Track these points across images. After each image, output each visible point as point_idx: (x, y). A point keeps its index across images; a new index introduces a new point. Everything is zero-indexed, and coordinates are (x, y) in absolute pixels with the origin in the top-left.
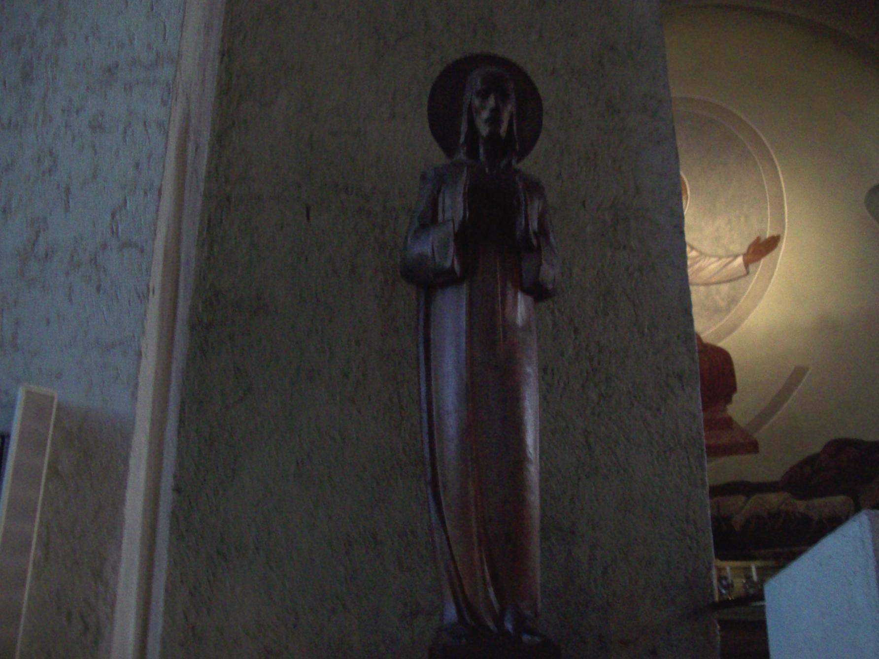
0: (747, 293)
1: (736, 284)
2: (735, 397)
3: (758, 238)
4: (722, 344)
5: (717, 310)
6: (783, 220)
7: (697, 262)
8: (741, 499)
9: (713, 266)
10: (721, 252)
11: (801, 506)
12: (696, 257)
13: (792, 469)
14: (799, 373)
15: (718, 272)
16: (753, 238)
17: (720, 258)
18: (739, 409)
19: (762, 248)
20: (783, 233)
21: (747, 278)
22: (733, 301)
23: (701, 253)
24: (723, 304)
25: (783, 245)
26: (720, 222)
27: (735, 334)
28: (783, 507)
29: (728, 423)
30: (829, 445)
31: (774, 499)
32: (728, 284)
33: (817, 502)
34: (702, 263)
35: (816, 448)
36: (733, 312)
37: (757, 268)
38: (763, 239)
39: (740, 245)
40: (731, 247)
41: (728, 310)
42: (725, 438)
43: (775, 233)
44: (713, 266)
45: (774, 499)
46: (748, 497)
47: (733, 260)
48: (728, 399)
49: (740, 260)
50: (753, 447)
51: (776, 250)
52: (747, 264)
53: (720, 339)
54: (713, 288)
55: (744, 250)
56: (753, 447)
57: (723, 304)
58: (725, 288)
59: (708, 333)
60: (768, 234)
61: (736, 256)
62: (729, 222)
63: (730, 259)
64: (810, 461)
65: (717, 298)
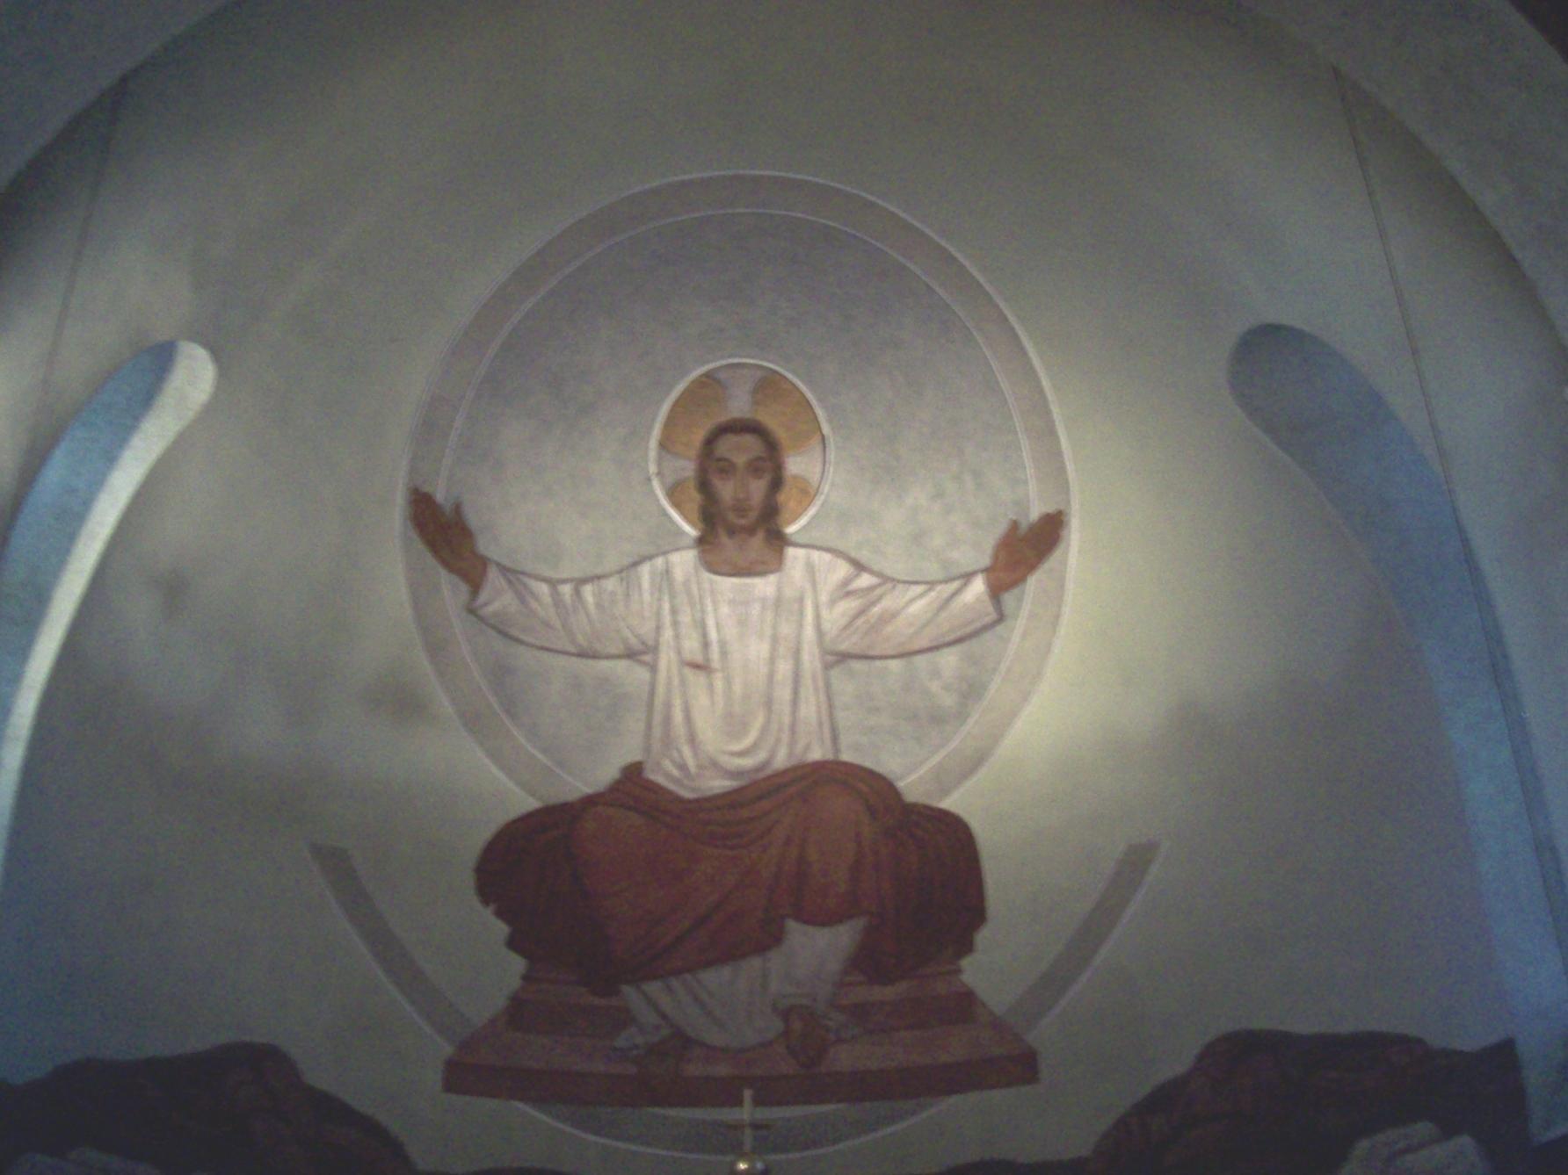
0: (1003, 668)
1: (974, 645)
2: (983, 937)
3: (1015, 525)
4: (947, 804)
5: (937, 718)
6: (1062, 469)
7: (873, 603)
9: (915, 608)
10: (933, 570)
12: (871, 589)
13: (1122, 1123)
14: (1136, 861)
15: (929, 622)
16: (1000, 529)
17: (931, 584)
18: (994, 967)
19: (1028, 547)
20: (1068, 502)
21: (999, 629)
22: (971, 691)
23: (885, 579)
24: (948, 701)
25: (1075, 536)
26: (918, 496)
27: (983, 772)
29: (965, 1005)
30: (1209, 1052)
32: (954, 649)
34: (888, 603)
35: (1176, 1060)
36: (971, 721)
37: (1020, 600)
38: (1024, 526)
39: (977, 551)
40: (955, 555)
41: (961, 715)
42: (955, 1047)
43: (1050, 508)
44: (915, 608)
47: (965, 584)
48: (965, 946)
49: (978, 586)
50: (1021, 1066)
51: (1057, 554)
52: (996, 591)
53: (946, 792)
54: (921, 661)
55: (986, 561)
56: (1021, 1066)
57: (948, 701)
58: (949, 660)
59: (914, 777)
60: (1035, 514)
61: (968, 577)
62: (939, 495)
63: (955, 585)
64: (1163, 1099)
65: (935, 686)
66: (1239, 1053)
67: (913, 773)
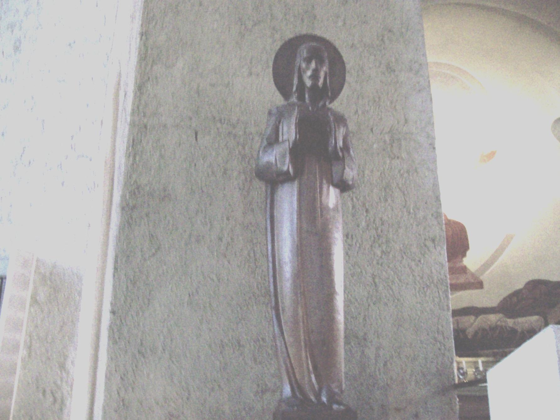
2: (468, 253)
8: (472, 318)
11: (510, 322)
18: (472, 261)
28: (499, 323)
29: (464, 270)
30: (528, 283)
31: (493, 318)
33: (520, 320)
35: (520, 285)
39: (370, 131)
45: (493, 318)
46: (477, 317)
48: (464, 255)
50: (480, 285)
56: (480, 285)
64: (516, 293)
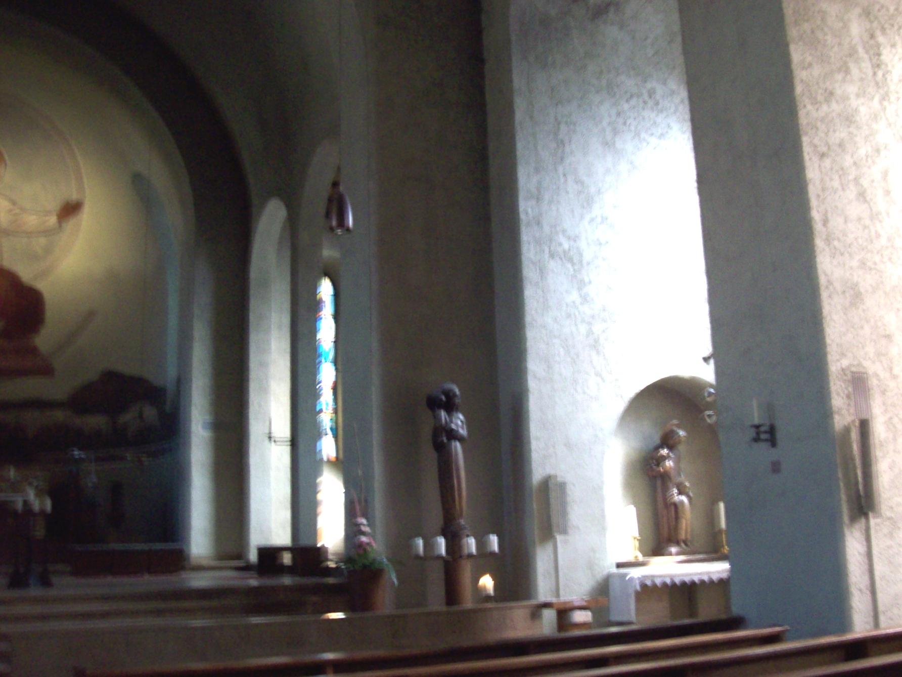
19: (70, 209)
22: (48, 250)
29: (34, 351)
31: (59, 415)
49: (53, 220)
50: (46, 370)
56: (46, 370)
58: (42, 241)
66: (110, 376)
67: (26, 273)
